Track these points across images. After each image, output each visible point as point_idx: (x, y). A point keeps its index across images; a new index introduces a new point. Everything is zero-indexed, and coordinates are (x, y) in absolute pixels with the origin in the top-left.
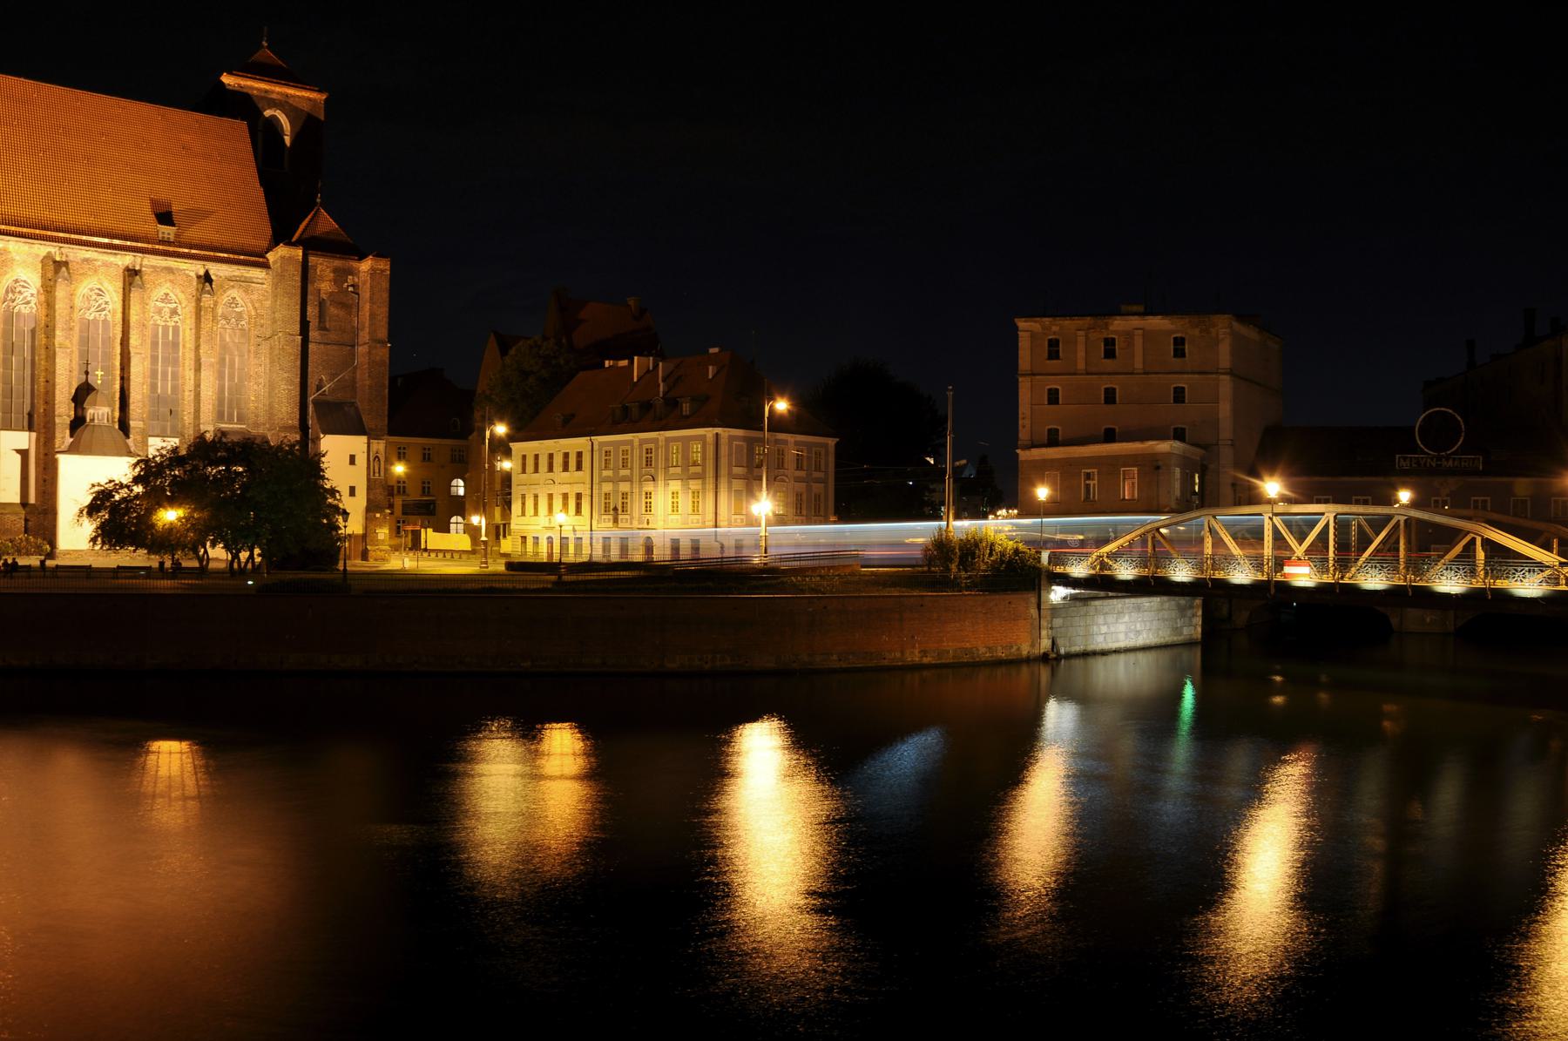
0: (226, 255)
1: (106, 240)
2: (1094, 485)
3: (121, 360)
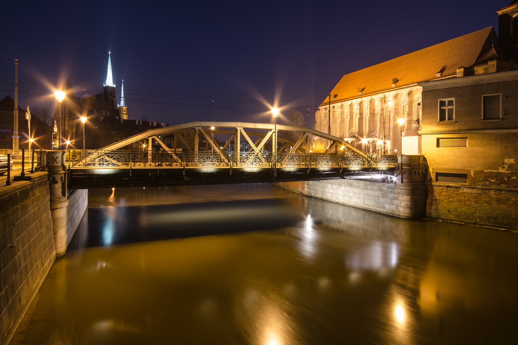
0: (451, 76)
1: (406, 86)
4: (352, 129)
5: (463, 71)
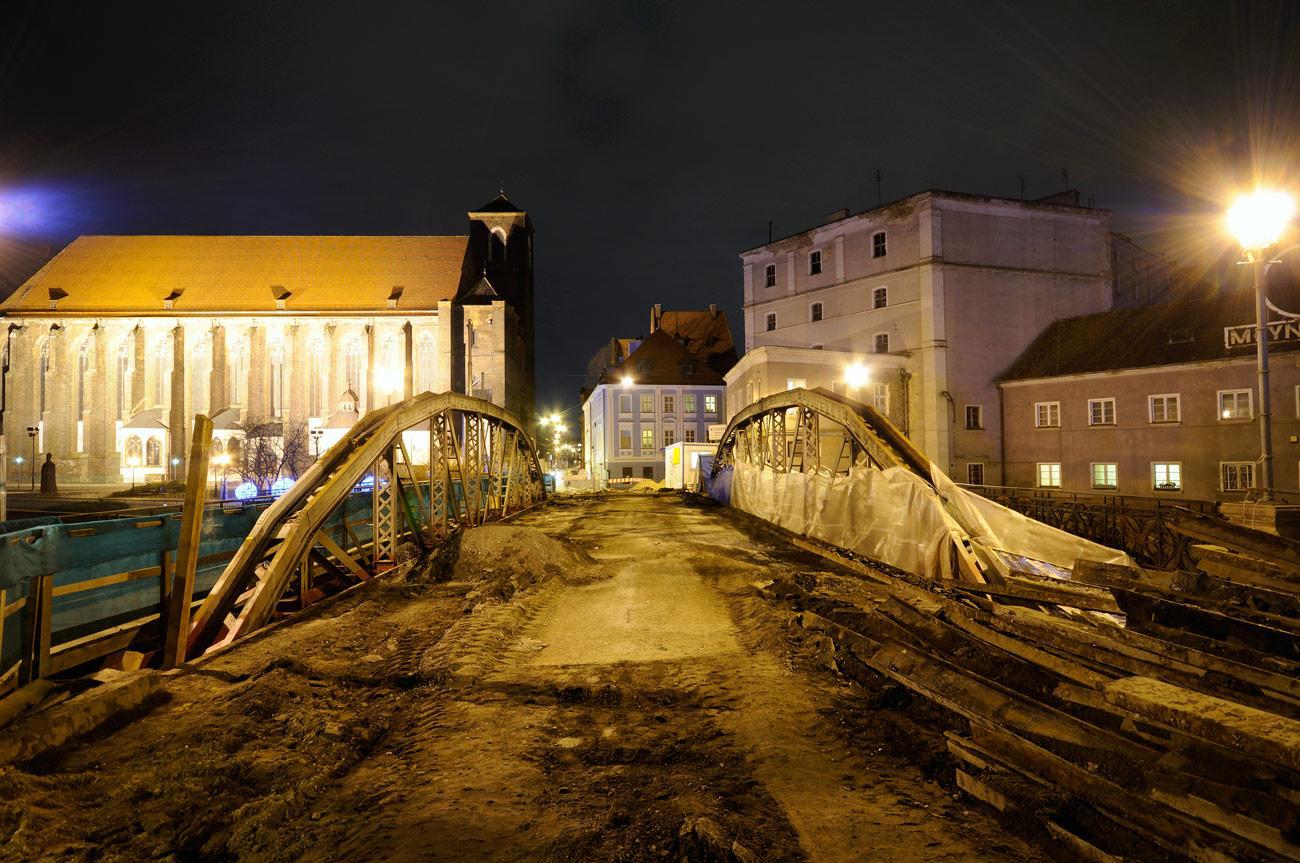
2: (1259, 467)
3: (793, 363)
4: (141, 403)
5: (450, 307)
